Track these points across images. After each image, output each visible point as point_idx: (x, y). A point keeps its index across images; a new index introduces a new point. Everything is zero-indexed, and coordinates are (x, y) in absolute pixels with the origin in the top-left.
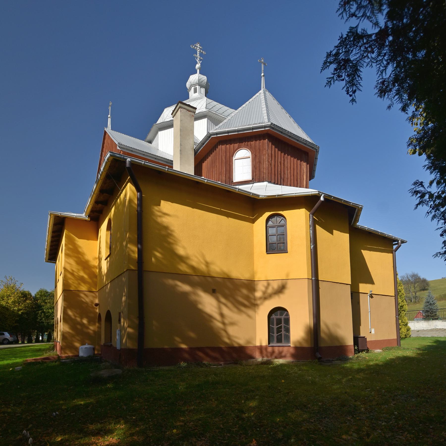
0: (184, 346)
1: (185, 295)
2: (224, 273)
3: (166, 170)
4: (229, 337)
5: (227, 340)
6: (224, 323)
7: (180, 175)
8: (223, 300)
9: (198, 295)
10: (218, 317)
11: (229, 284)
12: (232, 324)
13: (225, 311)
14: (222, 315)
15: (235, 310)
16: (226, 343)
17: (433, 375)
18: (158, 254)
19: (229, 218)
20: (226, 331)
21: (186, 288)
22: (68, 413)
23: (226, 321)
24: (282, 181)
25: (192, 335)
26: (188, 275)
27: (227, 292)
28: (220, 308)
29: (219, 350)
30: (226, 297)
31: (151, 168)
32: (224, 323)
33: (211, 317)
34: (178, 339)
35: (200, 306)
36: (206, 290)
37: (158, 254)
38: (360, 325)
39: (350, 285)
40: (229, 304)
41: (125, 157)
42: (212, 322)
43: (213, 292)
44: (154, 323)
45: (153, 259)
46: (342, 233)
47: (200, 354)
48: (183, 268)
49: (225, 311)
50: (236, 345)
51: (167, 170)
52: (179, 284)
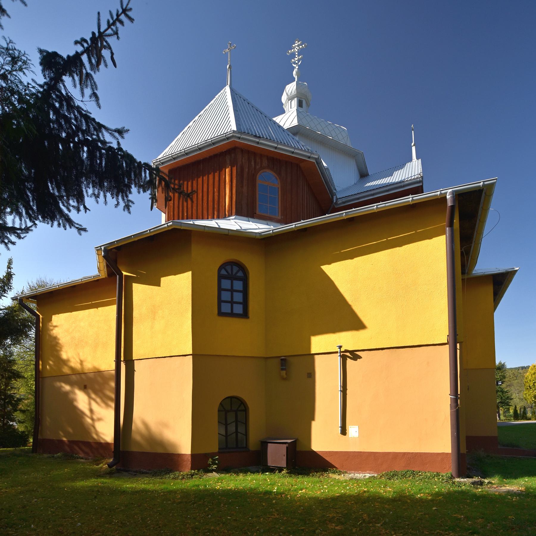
0: (65, 439)
1: (67, 393)
2: (95, 368)
3: (374, 209)
4: (97, 433)
5: (95, 436)
6: (93, 419)
7: (327, 222)
8: (93, 396)
9: (75, 394)
10: (87, 412)
11: (99, 379)
12: (99, 419)
13: (95, 406)
14: (91, 411)
15: (103, 405)
16: (94, 439)
17: (221, 513)
18: (51, 362)
19: (99, 308)
20: (94, 427)
21: (67, 388)
22: (381, 524)
23: (95, 417)
24: (205, 212)
25: (70, 430)
26: (67, 376)
27: (97, 387)
28: (90, 404)
29: (88, 444)
30: (96, 393)
31: (281, 233)
32: (93, 419)
33: (83, 413)
34: (61, 433)
35: (75, 403)
36: (80, 389)
37: (51, 362)
38: (313, 419)
39: (192, 356)
40: (98, 400)
41: (443, 192)
42: (83, 418)
43: (84, 388)
44: (48, 419)
45: (48, 367)
46: (177, 276)
47: (76, 448)
48: (66, 370)
49: (95, 406)
50: (102, 441)
51: (377, 208)
52: (63, 385)
